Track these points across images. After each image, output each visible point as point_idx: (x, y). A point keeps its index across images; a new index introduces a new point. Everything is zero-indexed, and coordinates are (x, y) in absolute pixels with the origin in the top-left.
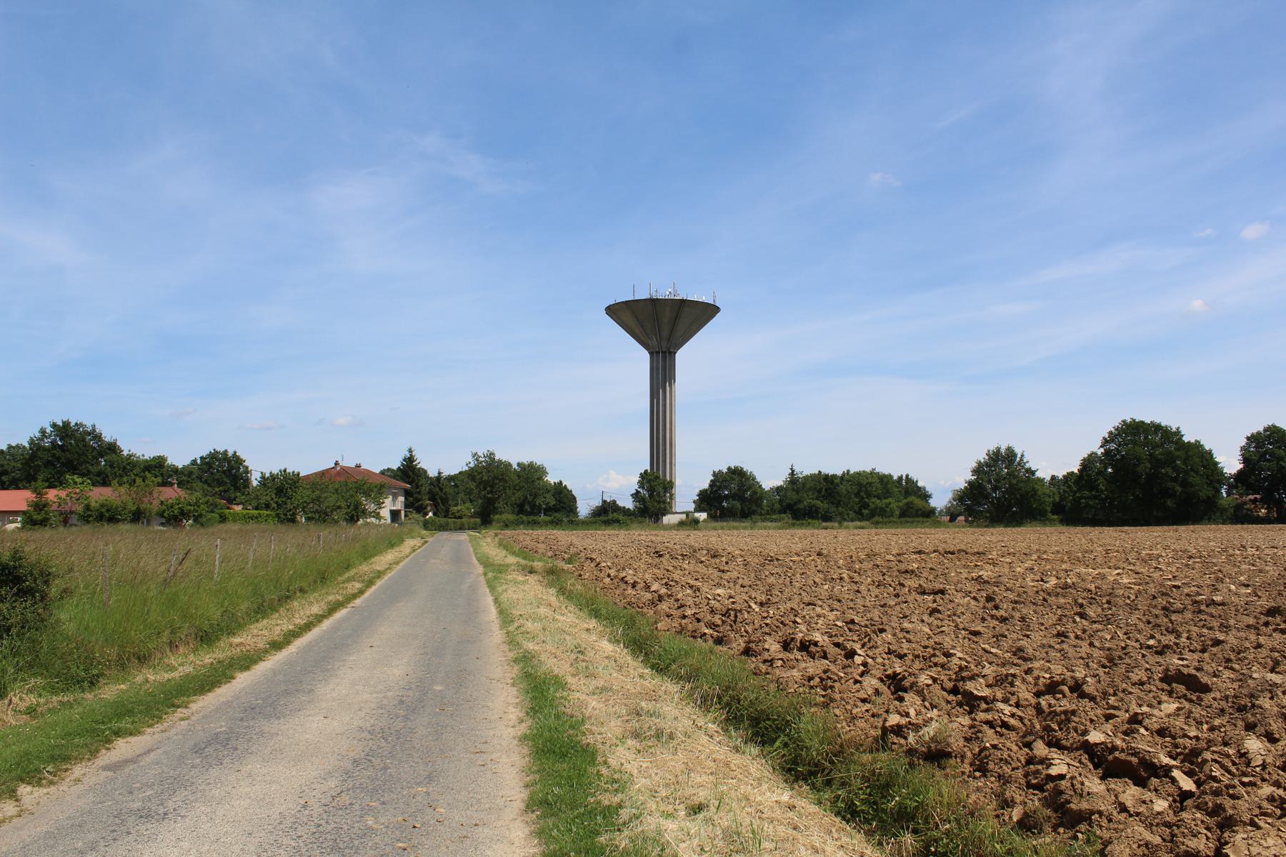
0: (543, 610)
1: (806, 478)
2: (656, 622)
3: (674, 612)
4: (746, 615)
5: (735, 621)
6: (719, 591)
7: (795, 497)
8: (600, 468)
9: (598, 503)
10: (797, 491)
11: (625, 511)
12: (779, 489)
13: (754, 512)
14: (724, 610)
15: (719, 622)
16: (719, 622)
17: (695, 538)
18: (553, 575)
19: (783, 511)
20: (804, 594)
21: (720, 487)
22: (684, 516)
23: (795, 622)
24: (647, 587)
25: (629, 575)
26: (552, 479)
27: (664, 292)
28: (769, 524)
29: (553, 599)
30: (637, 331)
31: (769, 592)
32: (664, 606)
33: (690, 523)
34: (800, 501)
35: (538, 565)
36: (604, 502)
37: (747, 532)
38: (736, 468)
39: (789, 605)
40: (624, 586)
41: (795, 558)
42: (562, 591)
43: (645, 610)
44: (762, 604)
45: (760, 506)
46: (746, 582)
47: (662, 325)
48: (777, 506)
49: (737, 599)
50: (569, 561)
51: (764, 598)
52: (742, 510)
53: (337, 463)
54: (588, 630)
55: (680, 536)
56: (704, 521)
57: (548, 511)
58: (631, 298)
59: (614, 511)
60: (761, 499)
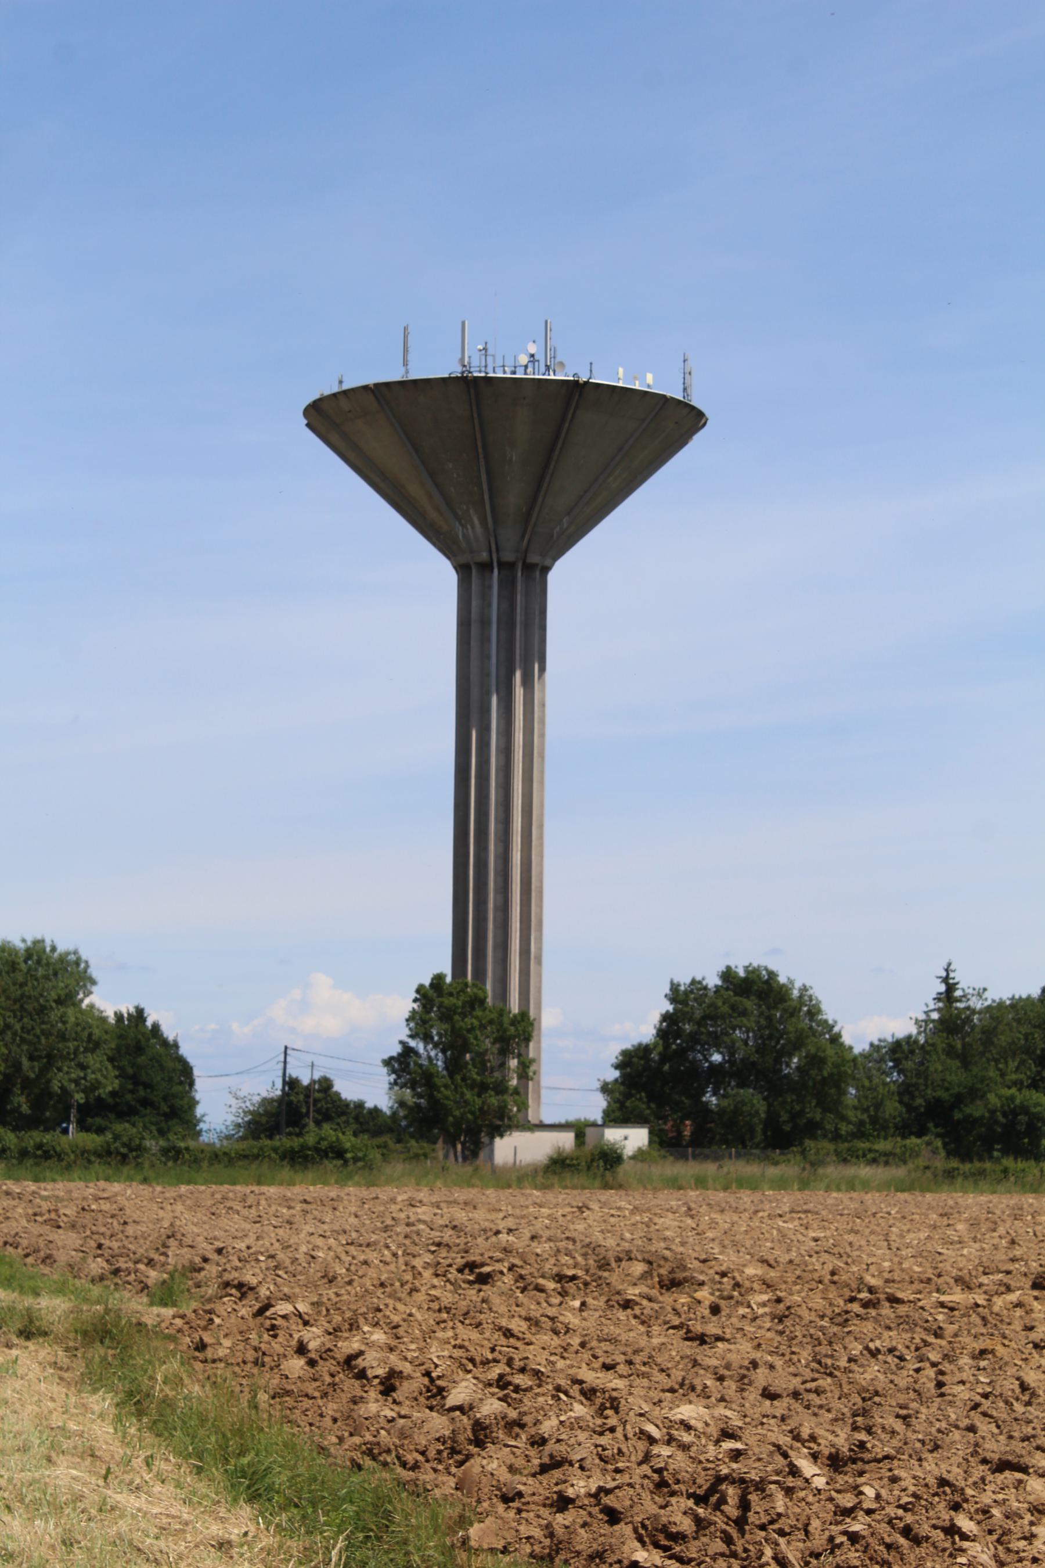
0: (66, 1474)
1: (997, 1011)
2: (463, 1522)
3: (526, 1485)
4: (780, 1503)
5: (740, 1523)
6: (688, 1411)
7: (957, 1077)
8: (275, 968)
9: (266, 1086)
10: (965, 1059)
11: (363, 1118)
12: (899, 1050)
13: (812, 1129)
14: (704, 1482)
15: (686, 1525)
16: (686, 1525)
17: (606, 1218)
18: (103, 1346)
19: (914, 1124)
20: (985, 1427)
21: (694, 1039)
22: (566, 1140)
23: (951, 1530)
24: (435, 1392)
25: (372, 1347)
26: (108, 1000)
27: (512, 353)
28: (865, 1171)
29: (103, 1433)
30: (415, 490)
31: (861, 1417)
32: (492, 1463)
33: (588, 1163)
34: (974, 1093)
35: (53, 1307)
36: (291, 1084)
37: (786, 1200)
38: (753, 972)
39: (933, 1467)
40: (351, 1386)
41: (957, 1296)
42: (136, 1402)
43: (426, 1476)
44: (835, 1462)
45: (831, 1104)
46: (783, 1381)
47: (503, 474)
48: (892, 1108)
49: (750, 1439)
50: (165, 1295)
51: (842, 1440)
52: (772, 1121)
53: (703, 979)
54: (223, 1546)
55: (552, 1208)
56: (640, 1156)
57: (94, 1112)
58: (394, 374)
59: (325, 1117)
60: (837, 1081)
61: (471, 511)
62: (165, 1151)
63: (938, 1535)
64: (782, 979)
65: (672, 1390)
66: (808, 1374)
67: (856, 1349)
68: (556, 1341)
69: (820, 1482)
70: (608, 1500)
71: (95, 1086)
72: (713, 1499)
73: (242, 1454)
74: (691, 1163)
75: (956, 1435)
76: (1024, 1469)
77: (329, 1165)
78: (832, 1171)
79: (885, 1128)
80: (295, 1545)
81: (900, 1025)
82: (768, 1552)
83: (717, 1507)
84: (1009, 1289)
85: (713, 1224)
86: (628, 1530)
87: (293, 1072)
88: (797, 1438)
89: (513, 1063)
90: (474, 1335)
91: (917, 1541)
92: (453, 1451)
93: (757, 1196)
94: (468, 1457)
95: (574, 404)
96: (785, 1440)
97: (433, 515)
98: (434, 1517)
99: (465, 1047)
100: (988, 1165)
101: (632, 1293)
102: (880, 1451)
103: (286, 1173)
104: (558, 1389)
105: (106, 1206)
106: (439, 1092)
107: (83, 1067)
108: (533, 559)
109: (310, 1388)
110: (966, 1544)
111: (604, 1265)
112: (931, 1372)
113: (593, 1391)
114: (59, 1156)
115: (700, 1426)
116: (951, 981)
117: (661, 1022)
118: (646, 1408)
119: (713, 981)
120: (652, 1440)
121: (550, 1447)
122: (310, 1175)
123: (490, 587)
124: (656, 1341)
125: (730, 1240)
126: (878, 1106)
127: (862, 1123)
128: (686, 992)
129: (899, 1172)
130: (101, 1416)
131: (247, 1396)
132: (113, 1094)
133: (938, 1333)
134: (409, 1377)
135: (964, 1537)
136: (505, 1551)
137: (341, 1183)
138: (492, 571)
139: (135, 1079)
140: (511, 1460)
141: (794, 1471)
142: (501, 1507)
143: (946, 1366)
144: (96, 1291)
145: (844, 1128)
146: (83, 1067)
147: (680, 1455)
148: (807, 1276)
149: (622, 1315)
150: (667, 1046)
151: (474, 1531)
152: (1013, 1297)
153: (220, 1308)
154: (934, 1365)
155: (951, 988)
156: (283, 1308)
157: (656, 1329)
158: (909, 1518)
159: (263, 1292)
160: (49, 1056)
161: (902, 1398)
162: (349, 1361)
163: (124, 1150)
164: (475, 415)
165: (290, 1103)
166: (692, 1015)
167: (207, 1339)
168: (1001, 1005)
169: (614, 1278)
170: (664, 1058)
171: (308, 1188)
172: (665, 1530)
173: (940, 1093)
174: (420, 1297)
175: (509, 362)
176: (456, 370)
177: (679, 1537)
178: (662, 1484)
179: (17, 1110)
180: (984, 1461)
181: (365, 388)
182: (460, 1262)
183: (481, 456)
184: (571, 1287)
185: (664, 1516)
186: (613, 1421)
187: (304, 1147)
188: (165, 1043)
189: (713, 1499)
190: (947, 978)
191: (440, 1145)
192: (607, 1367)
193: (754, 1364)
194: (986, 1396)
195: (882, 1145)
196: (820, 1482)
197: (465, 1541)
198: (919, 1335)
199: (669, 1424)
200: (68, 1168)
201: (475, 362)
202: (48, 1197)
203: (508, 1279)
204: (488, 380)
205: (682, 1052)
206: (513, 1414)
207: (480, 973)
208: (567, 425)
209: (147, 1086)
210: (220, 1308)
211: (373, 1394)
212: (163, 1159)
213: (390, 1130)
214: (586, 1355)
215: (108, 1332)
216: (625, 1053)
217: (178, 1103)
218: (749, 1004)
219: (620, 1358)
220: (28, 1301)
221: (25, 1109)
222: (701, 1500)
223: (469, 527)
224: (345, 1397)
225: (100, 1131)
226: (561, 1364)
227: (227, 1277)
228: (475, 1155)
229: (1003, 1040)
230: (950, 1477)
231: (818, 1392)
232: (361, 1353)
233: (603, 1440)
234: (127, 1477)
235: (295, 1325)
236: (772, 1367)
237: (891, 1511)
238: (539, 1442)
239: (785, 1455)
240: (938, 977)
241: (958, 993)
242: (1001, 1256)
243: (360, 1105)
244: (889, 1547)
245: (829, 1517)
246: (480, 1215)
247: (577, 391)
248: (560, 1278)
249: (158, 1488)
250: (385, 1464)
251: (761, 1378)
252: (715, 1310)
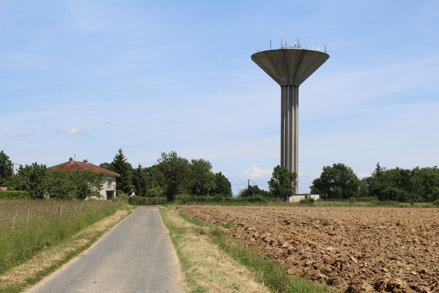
0: (210, 259)
1: (388, 172)
2: (286, 269)
4: (349, 265)
5: (341, 269)
6: (330, 248)
7: (380, 185)
8: (247, 164)
9: (245, 187)
10: (382, 181)
11: (264, 193)
12: (368, 180)
13: (351, 195)
14: (333, 262)
15: (330, 270)
16: (330, 270)
17: (311, 212)
18: (216, 235)
20: (388, 252)
21: (328, 178)
22: (303, 197)
23: (382, 271)
24: (280, 245)
26: (215, 171)
27: (291, 45)
28: (362, 203)
29: (216, 252)
30: (273, 71)
31: (363, 250)
32: (292, 258)
34: (383, 188)
35: (206, 229)
36: (250, 187)
37: (347, 209)
39: (378, 259)
40: (264, 244)
41: (381, 227)
42: (222, 246)
43: (279, 260)
44: (359, 258)
45: (355, 190)
46: (348, 243)
47: (289, 67)
48: (367, 191)
49: (342, 254)
50: (227, 226)
51: (360, 254)
53: (140, 166)
54: (240, 273)
55: (301, 210)
56: (318, 200)
57: (212, 192)
60: (356, 186)
62: (226, 199)
63: (380, 272)
64: (345, 166)
65: (326, 244)
66: (353, 242)
67: (362, 237)
68: (303, 235)
69: (356, 262)
70: (315, 265)
71: (212, 187)
72: (335, 265)
73: (243, 256)
74: (328, 202)
75: (382, 253)
76: (396, 260)
77: (257, 202)
78: (356, 203)
79: (366, 195)
80: (254, 273)
81: (369, 175)
82: (346, 275)
83: (336, 266)
84: (391, 226)
85: (333, 213)
86: (319, 271)
87: (250, 184)
88: (351, 253)
89: (293, 182)
90: (287, 234)
91: (376, 273)
92: (284, 256)
93: (341, 208)
94: (287, 257)
96: (349, 254)
97: (276, 76)
98: (281, 268)
99: (283, 179)
100: (386, 202)
101: (317, 226)
102: (368, 256)
103: (249, 204)
104: (304, 244)
105: (215, 210)
107: (210, 183)
108: (296, 84)
109: (256, 244)
110: (385, 273)
111: (312, 221)
112: (377, 241)
113: (311, 245)
114: (206, 200)
115: (332, 251)
118: (321, 248)
119: (332, 166)
120: (323, 254)
121: (303, 255)
122: (254, 204)
124: (323, 235)
125: (336, 216)
126: (364, 190)
127: (361, 194)
129: (369, 203)
130: (216, 249)
131: (244, 245)
132: (216, 189)
133: (378, 234)
134: (275, 242)
135: (385, 272)
136: (295, 274)
137: (260, 205)
139: (220, 186)
140: (295, 257)
141: (351, 260)
142: (294, 266)
143: (380, 240)
144: (214, 226)
145: (358, 195)
146: (210, 183)
147: (328, 257)
148: (352, 223)
149: (316, 230)
150: (323, 179)
151: (289, 271)
152: (392, 227)
153: (238, 229)
154: (377, 240)
155: (379, 167)
156: (250, 229)
157: (322, 233)
158: (374, 269)
159: (246, 226)
160: (204, 181)
161: (371, 246)
162: (263, 239)
166: (328, 173)
167: (235, 234)
168: (388, 171)
169: (314, 223)
170: (322, 181)
171: (253, 207)
172: (326, 271)
173: (377, 188)
174: (276, 227)
175: (291, 46)
176: (280, 48)
177: (329, 272)
178: (325, 262)
179: (198, 192)
180: (388, 258)
182: (284, 220)
184: (305, 225)
185: (326, 268)
186: (315, 250)
187: (253, 199)
188: (225, 179)
189: (335, 265)
191: (279, 198)
192: (313, 240)
193: (342, 240)
194: (388, 246)
195: (365, 198)
196: (356, 262)
197: (287, 273)
198: (374, 234)
199: (326, 251)
200: (207, 203)
201: (284, 47)
202: (162, 215)
203: (293, 224)
204: (286, 49)
205: (326, 180)
206: (295, 249)
207: (286, 165)
209: (222, 187)
210: (238, 229)
211: (268, 245)
213: (269, 196)
214: (309, 238)
215: (217, 233)
216: (315, 180)
217: (228, 190)
218: (339, 171)
219: (316, 238)
220: (201, 227)
221: (199, 191)
222: (332, 265)
224: (263, 246)
225: (213, 196)
226: (304, 239)
227: (239, 223)
228: (286, 200)
229: (389, 177)
230: (382, 261)
231: (355, 245)
232: (265, 237)
233: (313, 254)
234: (222, 260)
235: (252, 232)
236: (345, 240)
237: (370, 267)
238: (301, 254)
239: (349, 257)
240: (120, 151)
242: (390, 219)
243: (263, 191)
244: (370, 274)
245: (358, 268)
246: (287, 212)
247: (304, 51)
248: (303, 223)
249: (227, 262)
250: (271, 258)
251: (343, 242)
252: (334, 229)
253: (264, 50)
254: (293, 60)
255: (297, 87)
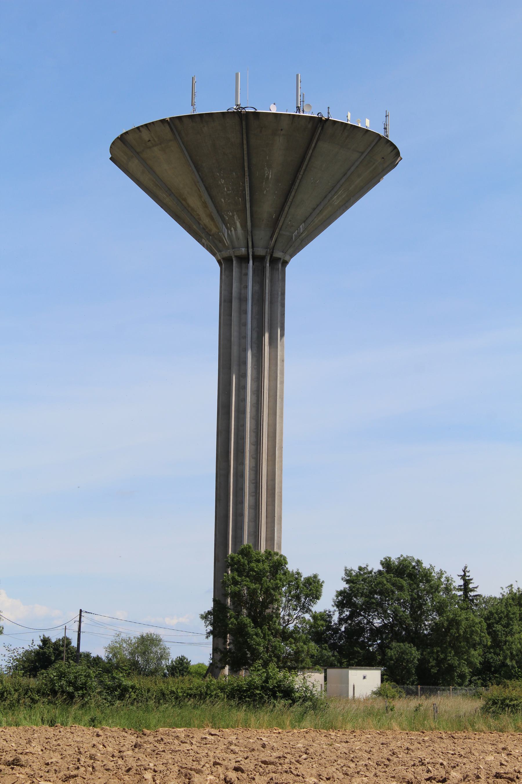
47: (254, 187)
61: (236, 217)
95: (317, 136)
97: (206, 221)
103: (240, 714)
106: (252, 639)
108: (278, 254)
116: (467, 578)
117: (337, 597)
123: (246, 274)
128: (357, 576)
138: (248, 263)
163: (71, 689)
164: (245, 142)
165: (45, 653)
181: (163, 121)
183: (247, 174)
190: (465, 575)
204: (256, 114)
208: (310, 152)
212: (109, 698)
223: (232, 229)
241: (471, 586)
247: (320, 126)
253: (167, 116)
254: (277, 155)
255: (279, 264)
